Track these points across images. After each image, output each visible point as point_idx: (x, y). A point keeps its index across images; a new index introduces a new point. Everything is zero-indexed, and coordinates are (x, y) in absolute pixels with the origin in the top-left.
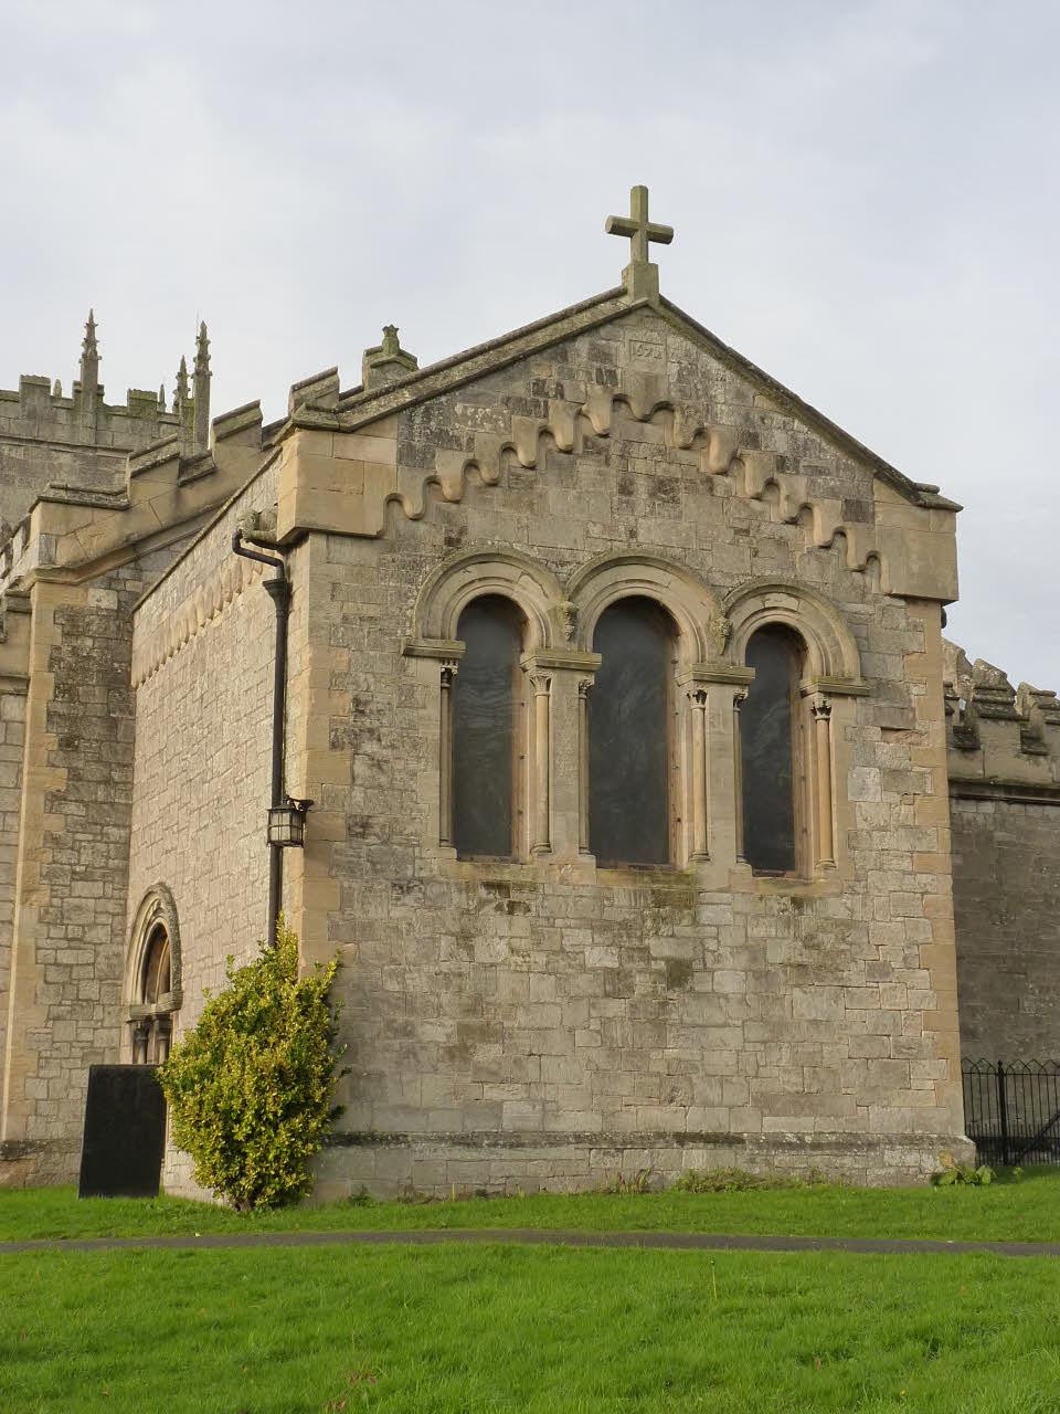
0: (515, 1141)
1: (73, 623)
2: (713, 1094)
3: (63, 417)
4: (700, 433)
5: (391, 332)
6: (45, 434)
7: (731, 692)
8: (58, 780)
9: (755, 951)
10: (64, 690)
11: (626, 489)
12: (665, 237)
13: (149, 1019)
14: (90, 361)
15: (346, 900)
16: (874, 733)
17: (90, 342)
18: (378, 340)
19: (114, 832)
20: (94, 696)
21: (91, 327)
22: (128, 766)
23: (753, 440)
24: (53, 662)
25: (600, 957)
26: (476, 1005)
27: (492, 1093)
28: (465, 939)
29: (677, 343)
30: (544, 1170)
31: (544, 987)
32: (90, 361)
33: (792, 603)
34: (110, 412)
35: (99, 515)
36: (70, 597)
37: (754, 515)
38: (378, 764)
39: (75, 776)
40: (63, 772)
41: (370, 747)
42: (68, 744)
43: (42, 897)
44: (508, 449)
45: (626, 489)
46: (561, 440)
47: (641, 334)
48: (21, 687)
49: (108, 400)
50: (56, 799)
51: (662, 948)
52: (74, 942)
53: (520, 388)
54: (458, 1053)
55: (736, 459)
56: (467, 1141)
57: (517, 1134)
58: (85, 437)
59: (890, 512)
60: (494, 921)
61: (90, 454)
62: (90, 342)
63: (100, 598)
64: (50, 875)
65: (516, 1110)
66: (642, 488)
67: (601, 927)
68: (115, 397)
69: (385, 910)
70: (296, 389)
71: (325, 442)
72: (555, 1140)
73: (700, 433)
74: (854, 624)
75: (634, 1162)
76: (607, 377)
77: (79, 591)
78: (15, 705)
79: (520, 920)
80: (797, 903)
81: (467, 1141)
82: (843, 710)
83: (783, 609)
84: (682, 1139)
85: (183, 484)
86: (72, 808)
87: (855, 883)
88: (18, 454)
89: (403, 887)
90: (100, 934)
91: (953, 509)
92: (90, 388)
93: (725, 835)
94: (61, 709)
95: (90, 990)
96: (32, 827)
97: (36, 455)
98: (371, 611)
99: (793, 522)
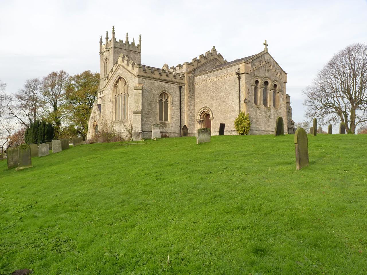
0: (260, 131)
1: (189, 77)
2: (271, 127)
3: (124, 45)
4: (271, 65)
5: (214, 47)
6: (122, 48)
7: (273, 90)
8: (189, 95)
9: (274, 115)
10: (189, 85)
11: (265, 70)
12: (268, 45)
13: (201, 121)
14: (127, 38)
15: (248, 108)
16: (282, 95)
17: (127, 35)
18: (213, 48)
19: (194, 101)
20: (191, 86)
21: (127, 33)
22: (194, 94)
23: (274, 66)
24: (188, 82)
25: (264, 115)
26: (257, 119)
27: (258, 126)
28: (256, 112)
29: (269, 56)
30: (262, 133)
31: (261, 117)
32: (127, 38)
33: (276, 82)
34: (117, 42)
35: (191, 66)
36: (189, 75)
37: (274, 73)
38: (250, 96)
39: (190, 95)
40: (189, 94)
41: (249, 94)
42: (190, 91)
43: (188, 108)
44: (258, 66)
45: (265, 70)
46: (262, 65)
47: (267, 55)
48: (184, 85)
49: (117, 40)
50: (189, 97)
51: (268, 114)
52: (191, 113)
53: (259, 60)
54: (256, 123)
55: (273, 68)
56: (257, 130)
57: (260, 130)
58: (127, 48)
59: (283, 74)
60: (258, 111)
61: (128, 51)
62: (127, 35)
63: (191, 75)
64: (189, 105)
65: (259, 128)
66: (266, 70)
67: (264, 112)
68: (117, 40)
69: (251, 109)
70: (207, 52)
71: (246, 64)
72: (262, 131)
73: (271, 65)
74: (281, 84)
75: (267, 133)
76: (264, 59)
77: (189, 74)
78: (40, 79)
79: (259, 111)
80: (277, 110)
81: (257, 130)
82: (280, 92)
83: (276, 83)
84: (270, 131)
85: (198, 63)
86: (190, 98)
87: (280, 109)
88: (119, 50)
89: (252, 107)
90: (193, 112)
91: (287, 74)
92: (127, 42)
93: (262, 103)
94: (189, 87)
95: (192, 118)
96: (187, 100)
97: (121, 51)
98: (249, 81)
99: (276, 74)
